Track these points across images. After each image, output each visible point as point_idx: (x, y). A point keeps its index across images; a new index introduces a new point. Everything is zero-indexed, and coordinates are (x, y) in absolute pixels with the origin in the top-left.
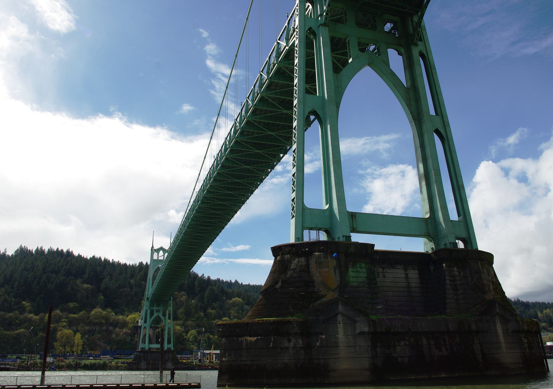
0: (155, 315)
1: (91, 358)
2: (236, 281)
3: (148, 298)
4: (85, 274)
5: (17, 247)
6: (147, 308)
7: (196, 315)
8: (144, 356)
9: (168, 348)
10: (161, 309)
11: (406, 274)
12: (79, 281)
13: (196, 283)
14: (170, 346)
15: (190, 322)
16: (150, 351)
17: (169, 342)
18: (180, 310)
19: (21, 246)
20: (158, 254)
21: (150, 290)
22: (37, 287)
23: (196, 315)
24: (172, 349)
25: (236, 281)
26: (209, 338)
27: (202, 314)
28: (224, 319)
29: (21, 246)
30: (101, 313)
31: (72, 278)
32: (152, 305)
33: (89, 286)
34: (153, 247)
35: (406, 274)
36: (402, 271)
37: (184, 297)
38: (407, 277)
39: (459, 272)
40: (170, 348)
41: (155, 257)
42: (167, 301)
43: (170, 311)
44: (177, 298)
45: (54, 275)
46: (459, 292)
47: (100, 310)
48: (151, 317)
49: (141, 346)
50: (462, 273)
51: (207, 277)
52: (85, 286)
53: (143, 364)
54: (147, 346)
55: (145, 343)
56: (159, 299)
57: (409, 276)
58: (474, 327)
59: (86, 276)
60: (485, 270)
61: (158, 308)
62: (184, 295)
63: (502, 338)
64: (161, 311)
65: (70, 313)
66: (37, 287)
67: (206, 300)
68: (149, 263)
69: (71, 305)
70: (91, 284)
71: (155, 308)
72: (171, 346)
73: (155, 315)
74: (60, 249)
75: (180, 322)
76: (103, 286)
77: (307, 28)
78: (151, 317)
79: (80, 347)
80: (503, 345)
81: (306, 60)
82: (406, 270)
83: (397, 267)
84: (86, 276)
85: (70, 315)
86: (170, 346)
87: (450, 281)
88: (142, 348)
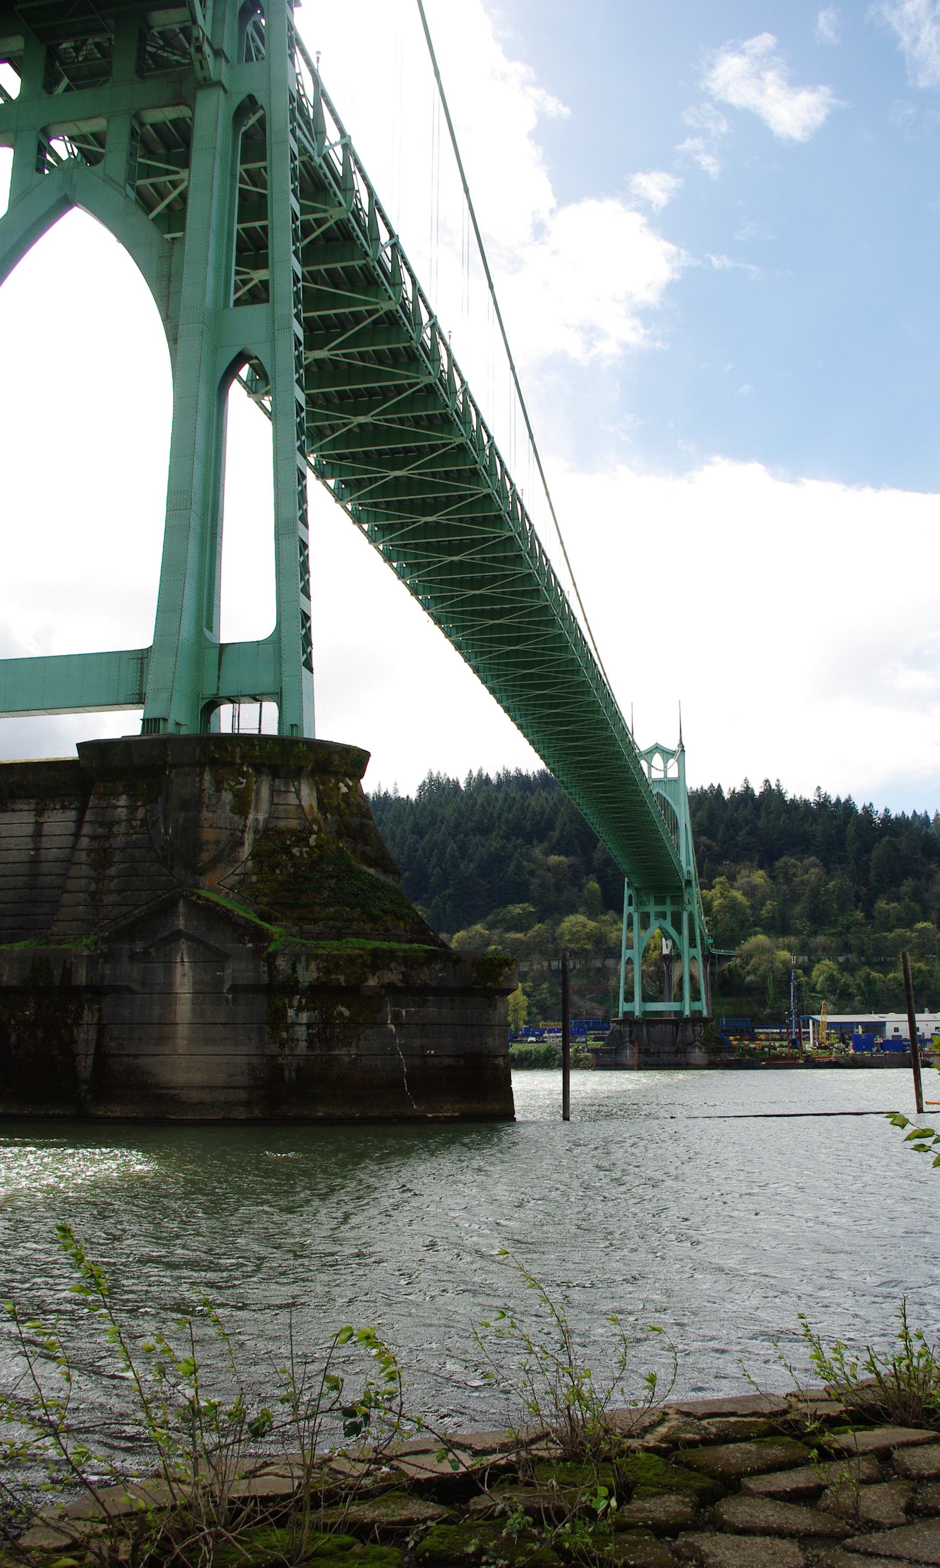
1: (530, 1039)
4: (553, 829)
5: (421, 777)
7: (842, 920)
8: (631, 1032)
11: (39, 825)
12: (537, 852)
13: (851, 830)
14: (697, 1006)
15: (820, 940)
16: (650, 1019)
17: (696, 997)
18: (798, 909)
22: (435, 872)
23: (842, 920)
24: (705, 1013)
26: (869, 982)
27: (859, 915)
28: (920, 925)
30: (584, 926)
31: (520, 841)
33: (562, 858)
35: (39, 825)
36: (29, 817)
37: (813, 870)
38: (38, 834)
39: (132, 809)
40: (700, 1012)
43: (691, 915)
44: (794, 875)
45: (476, 840)
46: (113, 871)
47: (581, 918)
49: (623, 1007)
50: (140, 814)
51: (881, 812)
52: (554, 859)
53: (629, 1054)
54: (637, 1007)
55: (632, 1001)
57: (46, 829)
58: (81, 976)
59: (555, 834)
60: (227, 797)
61: (659, 908)
62: (814, 865)
63: (184, 1009)
65: (507, 930)
66: (435, 872)
67: (872, 875)
69: (517, 909)
70: (567, 854)
72: (703, 1007)
74: (513, 773)
75: (792, 940)
76: (597, 856)
79: (523, 1013)
80: (182, 1031)
81: (263, 159)
82: (39, 812)
83: (17, 807)
84: (555, 834)
85: (507, 935)
86: (697, 1006)
87: (93, 838)
88: (625, 1013)
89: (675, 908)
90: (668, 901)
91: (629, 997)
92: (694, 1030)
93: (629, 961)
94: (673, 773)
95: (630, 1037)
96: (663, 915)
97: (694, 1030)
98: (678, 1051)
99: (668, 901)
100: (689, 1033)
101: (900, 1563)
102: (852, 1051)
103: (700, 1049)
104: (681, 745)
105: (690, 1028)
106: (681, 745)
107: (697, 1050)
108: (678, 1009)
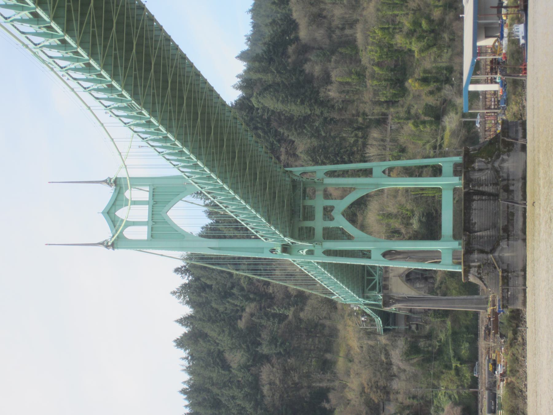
0: (340, 222)
2: (243, 56)
3: (286, 249)
5: (244, 40)
6: (318, 250)
8: (482, 251)
9: (456, 173)
10: (319, 203)
16: (465, 228)
17: (437, 171)
19: (184, 392)
20: (129, 224)
21: (266, 241)
25: (243, 56)
29: (184, 392)
32: (307, 235)
34: (105, 244)
40: (456, 165)
41: (140, 233)
42: (294, 184)
48: (349, 238)
49: (447, 265)
56: (292, 211)
61: (319, 214)
64: (329, 203)
68: (184, 253)
71: (319, 224)
73: (340, 222)
77: (323, 255)
78: (349, 238)
89: (320, 194)
90: (309, 202)
91: (435, 256)
92: (480, 170)
93: (388, 254)
94: (143, 194)
95: (487, 253)
96: (328, 212)
97: (480, 170)
98: (507, 189)
99: (309, 202)
100: (483, 176)
101: (359, 393)
102: (416, 106)
103: (503, 161)
104: (107, 182)
105: (476, 176)
106: (107, 182)
107: (505, 165)
108: (451, 193)
